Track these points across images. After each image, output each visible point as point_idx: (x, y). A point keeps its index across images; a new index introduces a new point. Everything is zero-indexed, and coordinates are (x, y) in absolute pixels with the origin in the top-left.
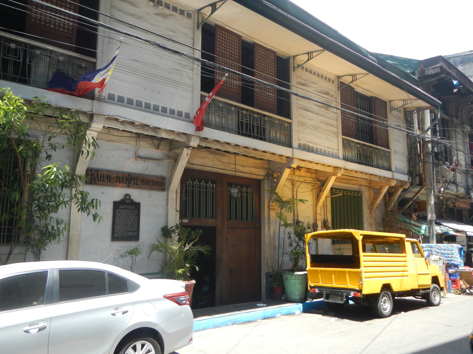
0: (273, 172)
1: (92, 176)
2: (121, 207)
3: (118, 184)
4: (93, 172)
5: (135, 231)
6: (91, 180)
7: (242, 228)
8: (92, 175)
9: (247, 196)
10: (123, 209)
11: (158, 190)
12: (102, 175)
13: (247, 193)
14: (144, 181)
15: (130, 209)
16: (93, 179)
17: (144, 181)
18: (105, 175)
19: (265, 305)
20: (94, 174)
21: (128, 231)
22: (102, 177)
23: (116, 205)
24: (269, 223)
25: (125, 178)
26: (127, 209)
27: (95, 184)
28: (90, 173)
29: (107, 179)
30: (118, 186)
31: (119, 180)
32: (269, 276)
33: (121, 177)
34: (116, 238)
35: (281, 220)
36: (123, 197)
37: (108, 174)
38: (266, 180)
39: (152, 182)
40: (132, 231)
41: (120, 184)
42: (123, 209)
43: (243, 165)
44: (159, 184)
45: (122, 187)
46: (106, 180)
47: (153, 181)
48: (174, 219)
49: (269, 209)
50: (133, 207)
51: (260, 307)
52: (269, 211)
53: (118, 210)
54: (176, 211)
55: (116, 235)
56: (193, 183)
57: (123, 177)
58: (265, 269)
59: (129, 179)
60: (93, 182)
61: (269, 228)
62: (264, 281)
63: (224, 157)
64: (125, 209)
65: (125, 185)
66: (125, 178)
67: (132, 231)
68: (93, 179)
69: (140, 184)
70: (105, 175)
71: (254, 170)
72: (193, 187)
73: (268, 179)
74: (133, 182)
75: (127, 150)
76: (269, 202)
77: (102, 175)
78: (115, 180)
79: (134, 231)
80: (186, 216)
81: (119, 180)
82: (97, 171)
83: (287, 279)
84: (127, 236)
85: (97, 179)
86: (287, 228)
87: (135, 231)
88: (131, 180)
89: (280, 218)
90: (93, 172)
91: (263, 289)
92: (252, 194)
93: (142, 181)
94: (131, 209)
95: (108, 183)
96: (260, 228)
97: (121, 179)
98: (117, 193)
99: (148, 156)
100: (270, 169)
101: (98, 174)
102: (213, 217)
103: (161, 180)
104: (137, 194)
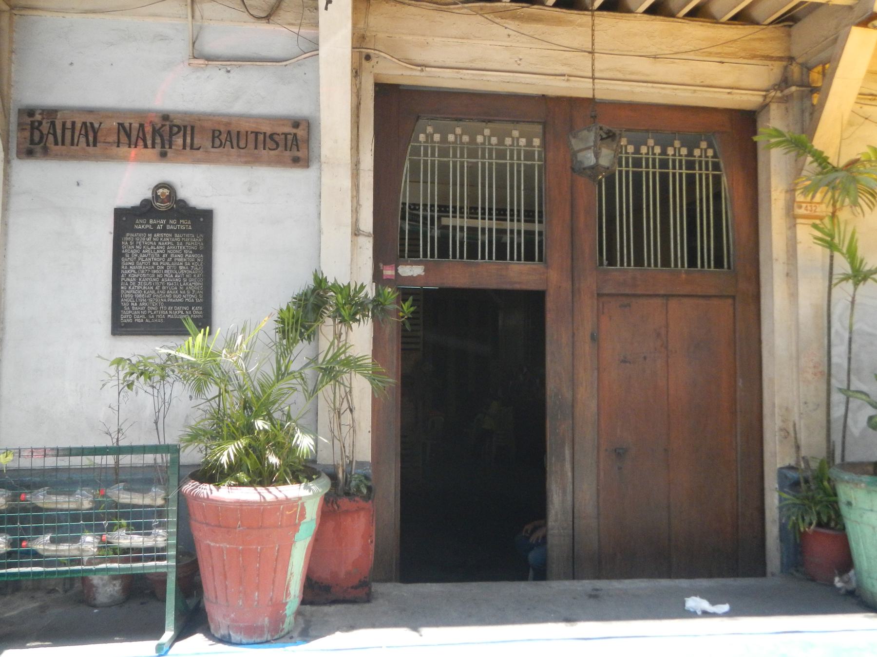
0: (809, 69)
1: (33, 128)
2: (141, 224)
3: (124, 149)
4: (38, 117)
5: (196, 304)
6: (32, 142)
7: (667, 296)
8: (35, 127)
9: (691, 179)
10: (147, 231)
11: (278, 162)
12: (69, 125)
13: (690, 165)
14: (223, 137)
15: (170, 231)
16: (37, 138)
17: (223, 137)
18: (78, 126)
19: (725, 608)
20: (40, 123)
21: (167, 304)
22: (68, 134)
23: (125, 220)
24: (791, 275)
25: (148, 129)
26: (164, 230)
27: (46, 153)
28: (28, 120)
29: (87, 136)
30: (125, 159)
31: (129, 136)
32: (792, 482)
33: (136, 125)
34: (127, 325)
35: (837, 254)
36: (149, 195)
37: (89, 119)
38: (773, 107)
39: (251, 137)
40: (184, 304)
41: (133, 151)
42: (147, 231)
43: (653, 50)
44: (287, 142)
45: (138, 160)
46: (83, 140)
47: (257, 134)
48: (350, 262)
49: (792, 217)
50: (186, 224)
51: (692, 615)
52: (793, 227)
53: (129, 237)
54: (356, 232)
55: (126, 317)
56: (444, 139)
57: (142, 126)
58: (777, 456)
59: (166, 134)
60: (38, 148)
61: (794, 296)
62: (773, 500)
63: (559, 29)
64: (154, 231)
65: (149, 151)
66: (148, 129)
67: (184, 304)
68: (37, 138)
69: (209, 144)
70: (78, 126)
71: (710, 70)
72: (444, 153)
73: (786, 99)
74: (179, 141)
75: (163, 38)
76: (791, 191)
77: (69, 125)
78: (113, 138)
79: (190, 305)
80: (414, 253)
81: (129, 136)
82: (51, 113)
83: (849, 504)
84: (166, 319)
85: (51, 137)
86: (861, 286)
87: (196, 304)
88: (171, 135)
89: (831, 246)
90: (38, 117)
91: (772, 531)
92: (716, 166)
93: (215, 135)
94: (179, 231)
95: (91, 149)
96: (757, 298)
97: (134, 134)
98: (131, 180)
99: (240, 52)
100: (791, 59)
101: (53, 124)
102: (530, 257)
103: (287, 130)
104: (197, 182)
